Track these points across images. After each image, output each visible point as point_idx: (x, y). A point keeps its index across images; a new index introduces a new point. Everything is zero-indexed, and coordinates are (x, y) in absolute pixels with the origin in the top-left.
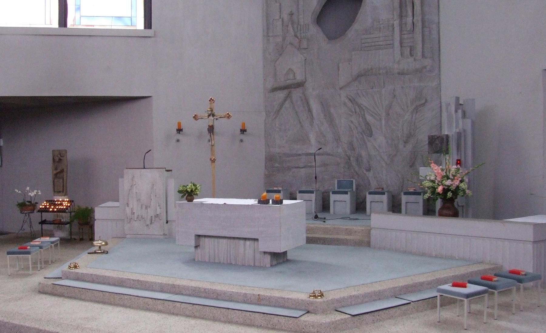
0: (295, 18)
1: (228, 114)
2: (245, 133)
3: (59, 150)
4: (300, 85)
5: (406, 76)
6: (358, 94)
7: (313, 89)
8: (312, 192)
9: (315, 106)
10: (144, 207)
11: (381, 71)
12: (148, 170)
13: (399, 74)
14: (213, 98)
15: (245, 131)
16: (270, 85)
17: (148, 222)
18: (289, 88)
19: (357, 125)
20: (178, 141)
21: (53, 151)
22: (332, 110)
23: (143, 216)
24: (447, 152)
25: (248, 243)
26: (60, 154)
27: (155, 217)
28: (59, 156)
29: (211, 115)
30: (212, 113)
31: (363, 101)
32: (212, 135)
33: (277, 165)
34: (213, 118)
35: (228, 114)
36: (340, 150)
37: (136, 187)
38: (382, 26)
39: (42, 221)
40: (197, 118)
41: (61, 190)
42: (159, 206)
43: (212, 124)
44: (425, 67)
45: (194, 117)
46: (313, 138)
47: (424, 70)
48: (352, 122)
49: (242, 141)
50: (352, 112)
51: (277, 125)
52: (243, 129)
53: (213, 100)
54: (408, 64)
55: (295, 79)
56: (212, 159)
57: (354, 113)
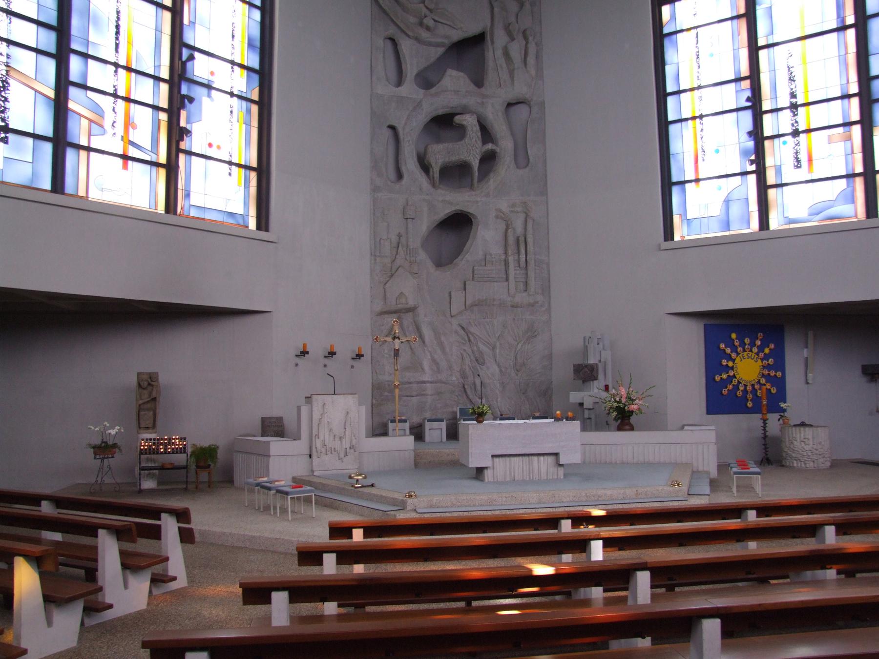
0: (403, 240)
3: (150, 373)
4: (412, 310)
5: (519, 309)
6: (470, 322)
7: (425, 316)
8: (442, 420)
9: (427, 332)
10: (337, 439)
11: (495, 303)
12: (339, 396)
13: (512, 306)
16: (379, 307)
17: (342, 455)
18: (398, 313)
19: (470, 353)
20: (297, 365)
21: (139, 374)
22: (443, 338)
23: (336, 450)
24: (595, 378)
25: (542, 458)
26: (150, 378)
27: (350, 448)
28: (149, 380)
31: (473, 330)
33: (386, 394)
36: (454, 378)
37: (327, 416)
38: (494, 260)
41: (150, 425)
42: (354, 436)
44: (537, 302)
46: (426, 364)
47: (537, 305)
48: (465, 350)
49: (352, 367)
50: (465, 341)
51: (386, 351)
54: (521, 298)
55: (407, 304)
57: (467, 342)
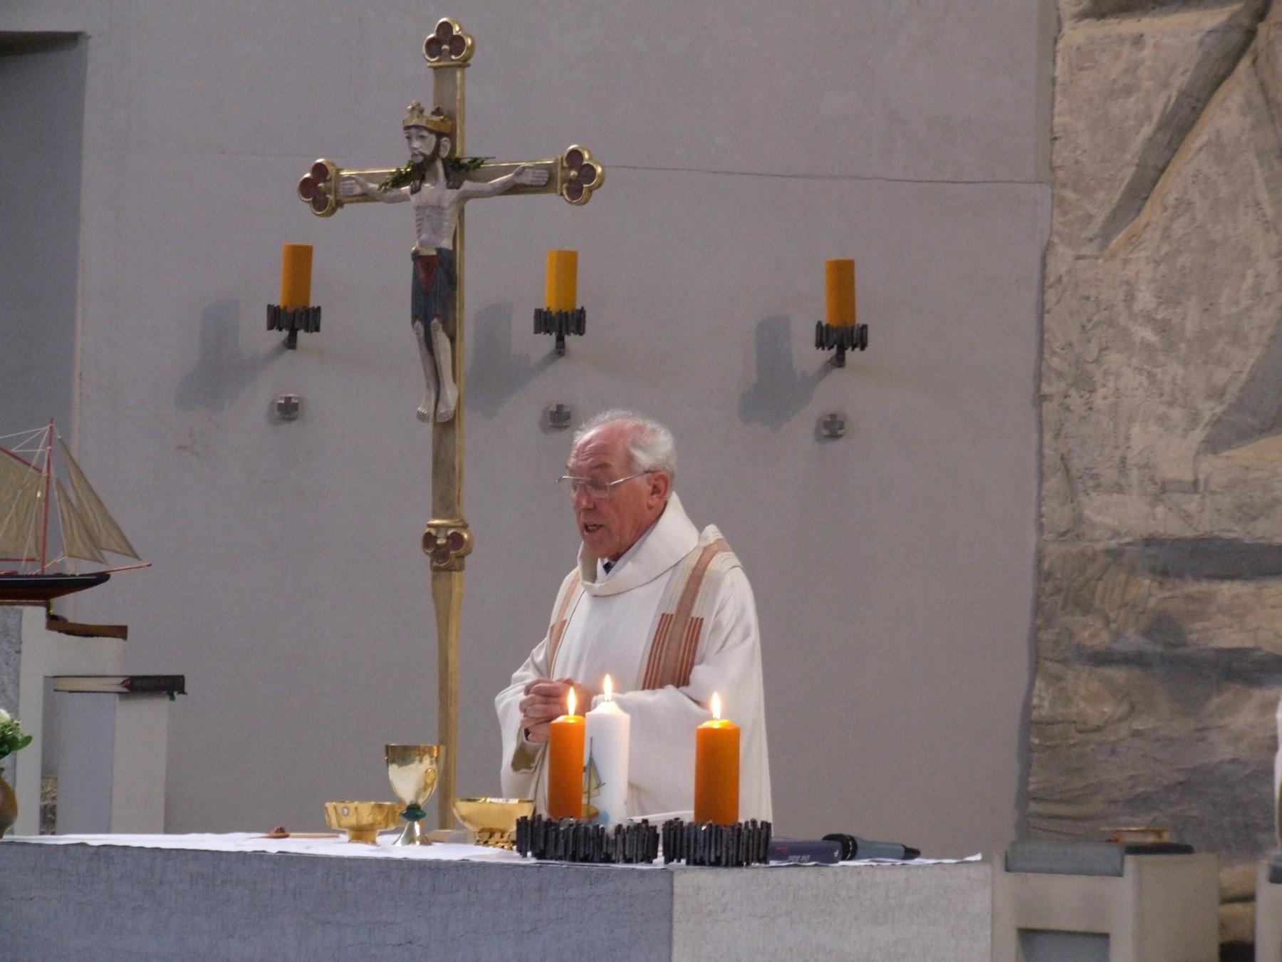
1: (575, 156)
2: (851, 355)
14: (457, 28)
15: (859, 338)
29: (439, 164)
30: (444, 153)
32: (442, 341)
34: (451, 195)
35: (575, 156)
39: (102, 548)
40: (331, 197)
43: (446, 244)
45: (307, 188)
51: (1145, 299)
52: (566, 308)
53: (457, 43)
56: (441, 541)
